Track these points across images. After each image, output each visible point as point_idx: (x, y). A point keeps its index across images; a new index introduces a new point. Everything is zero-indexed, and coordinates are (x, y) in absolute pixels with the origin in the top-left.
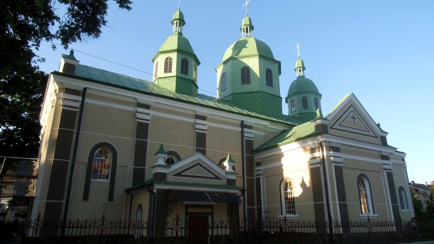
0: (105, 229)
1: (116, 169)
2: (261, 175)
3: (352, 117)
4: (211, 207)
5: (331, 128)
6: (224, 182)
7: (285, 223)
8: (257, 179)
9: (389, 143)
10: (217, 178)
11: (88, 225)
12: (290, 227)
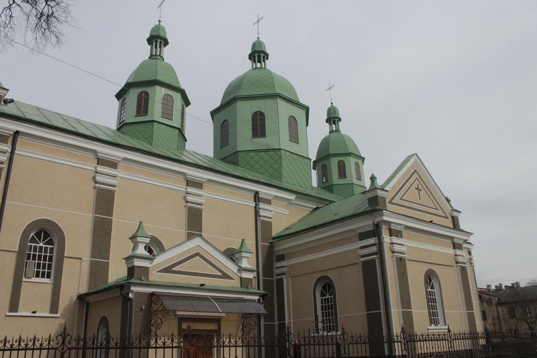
0: (68, 351)
1: (62, 263)
2: (284, 274)
3: (416, 189)
4: (217, 320)
5: (390, 202)
6: (235, 284)
7: (344, 339)
8: (278, 280)
9: (462, 227)
10: (225, 276)
11: (38, 344)
12: (350, 343)
